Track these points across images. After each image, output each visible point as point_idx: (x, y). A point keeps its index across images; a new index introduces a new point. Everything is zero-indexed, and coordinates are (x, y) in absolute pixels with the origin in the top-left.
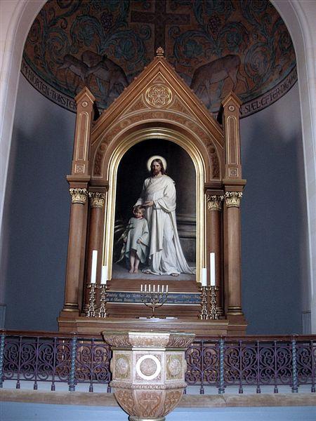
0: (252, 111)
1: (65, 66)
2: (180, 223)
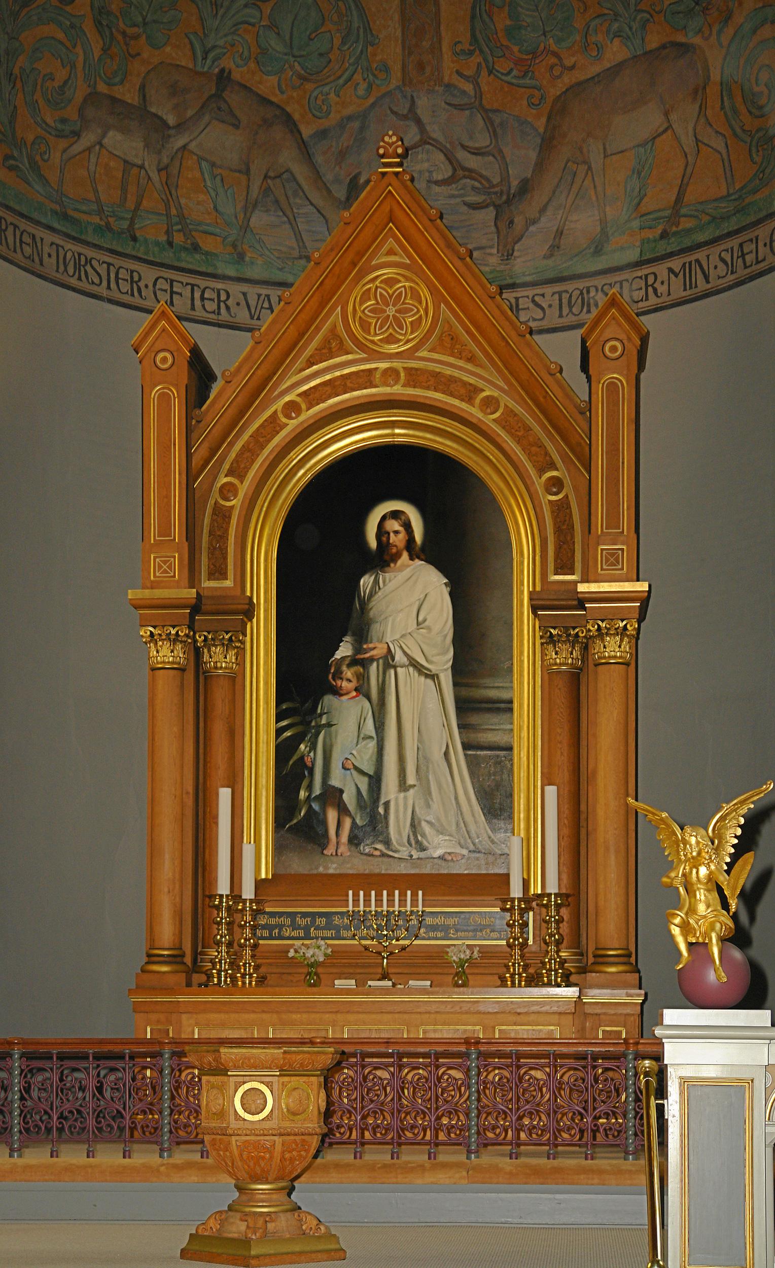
0: (741, 273)
1: (88, 139)
2: (464, 706)
